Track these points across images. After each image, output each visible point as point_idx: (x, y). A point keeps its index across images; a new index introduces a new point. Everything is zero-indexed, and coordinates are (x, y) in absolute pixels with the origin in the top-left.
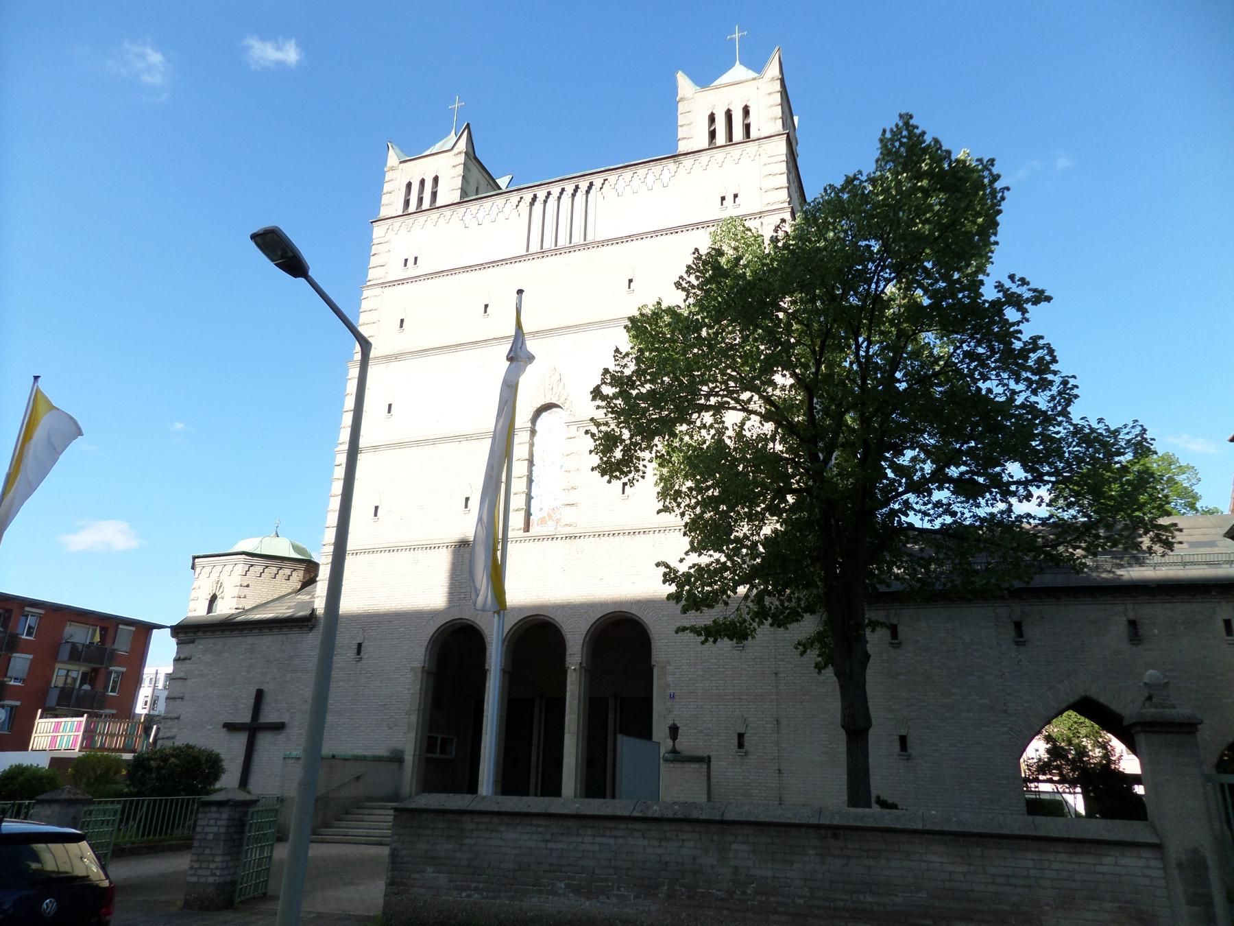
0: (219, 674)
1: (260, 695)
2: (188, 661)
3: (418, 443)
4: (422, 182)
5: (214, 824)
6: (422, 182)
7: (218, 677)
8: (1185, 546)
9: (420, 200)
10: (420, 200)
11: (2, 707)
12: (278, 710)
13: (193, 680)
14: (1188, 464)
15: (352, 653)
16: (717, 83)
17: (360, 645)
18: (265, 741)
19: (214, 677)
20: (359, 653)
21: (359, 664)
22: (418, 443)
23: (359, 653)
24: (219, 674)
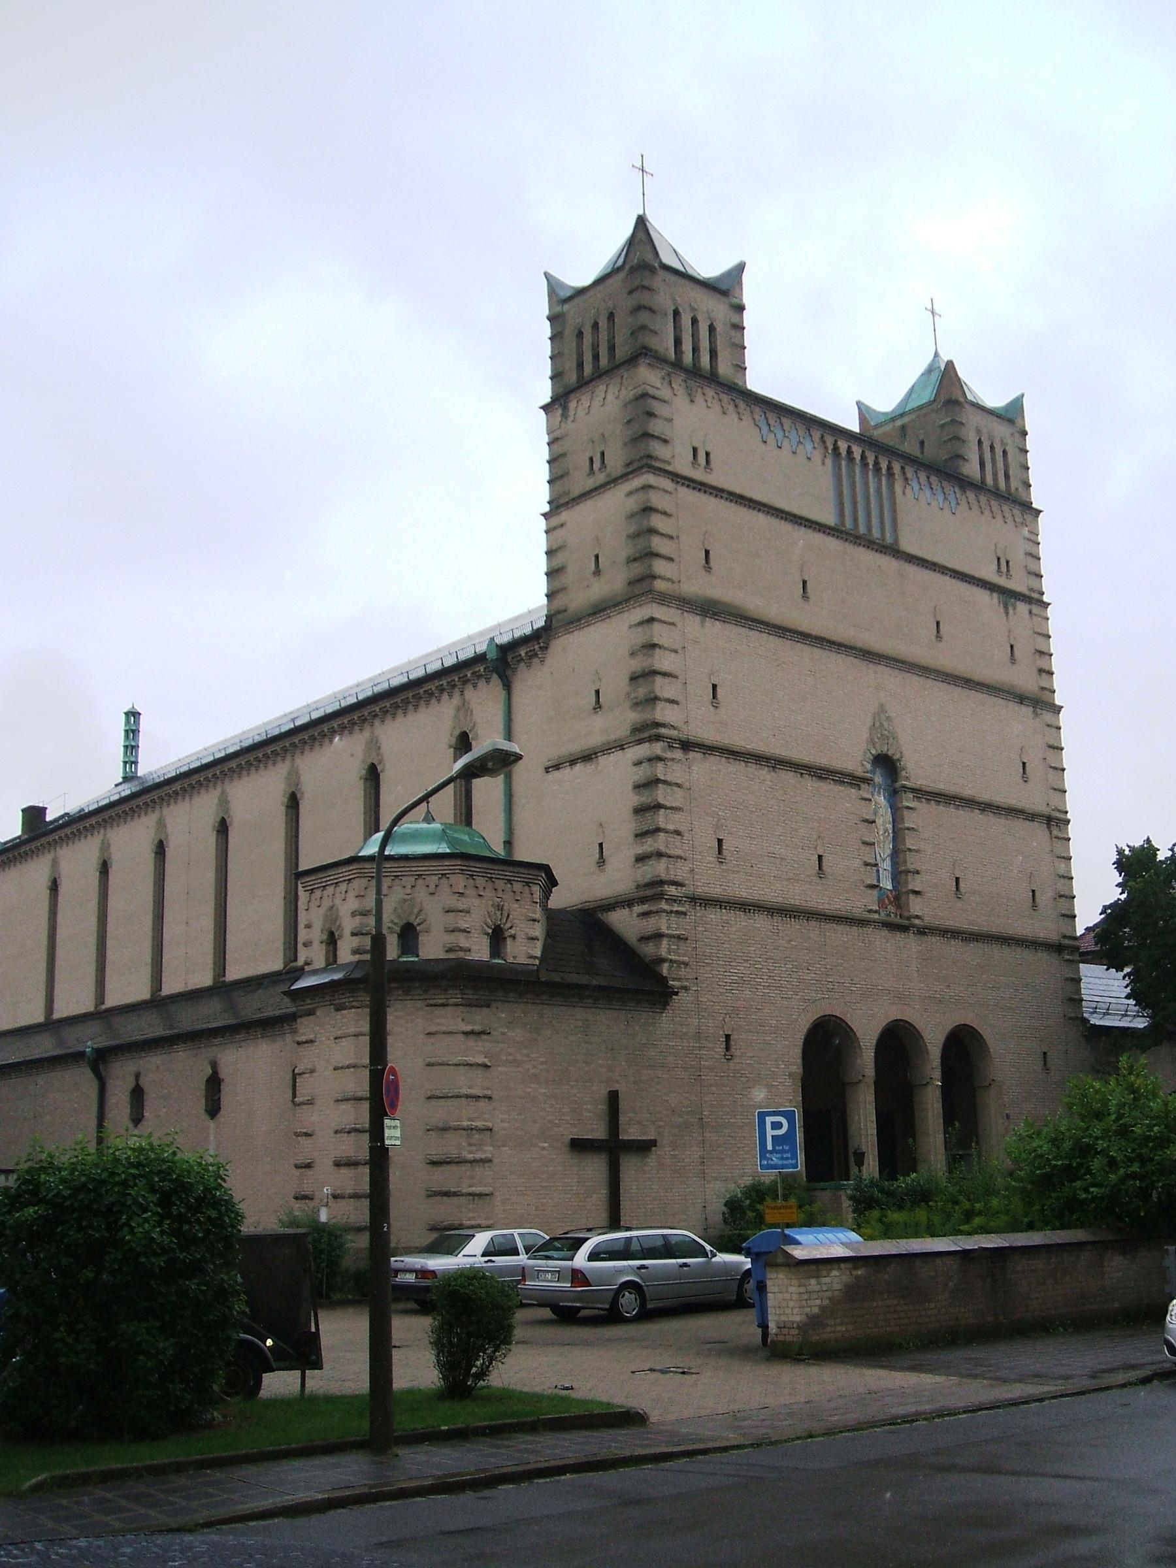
0: (542, 1063)
1: (613, 1098)
2: (484, 1037)
3: (759, 759)
4: (595, 326)
5: (787, 1333)
6: (595, 326)
7: (542, 1067)
8: (231, 747)
9: (596, 357)
10: (596, 357)
11: (1175, 1351)
12: (639, 1123)
13: (500, 1069)
14: (1159, 850)
15: (720, 1049)
16: (684, 270)
17: (728, 1037)
18: (630, 1167)
19: (534, 1067)
20: (728, 1048)
21: (731, 1064)
22: (759, 759)
23: (728, 1048)
24: (542, 1063)
